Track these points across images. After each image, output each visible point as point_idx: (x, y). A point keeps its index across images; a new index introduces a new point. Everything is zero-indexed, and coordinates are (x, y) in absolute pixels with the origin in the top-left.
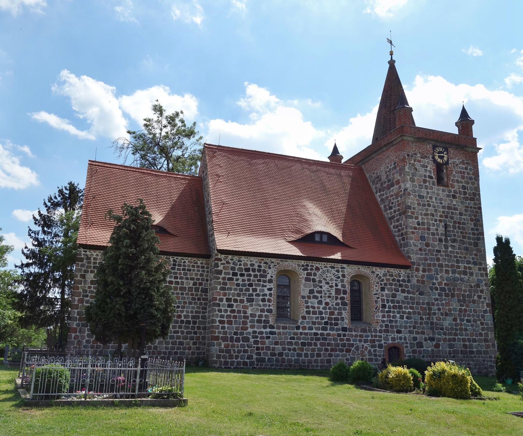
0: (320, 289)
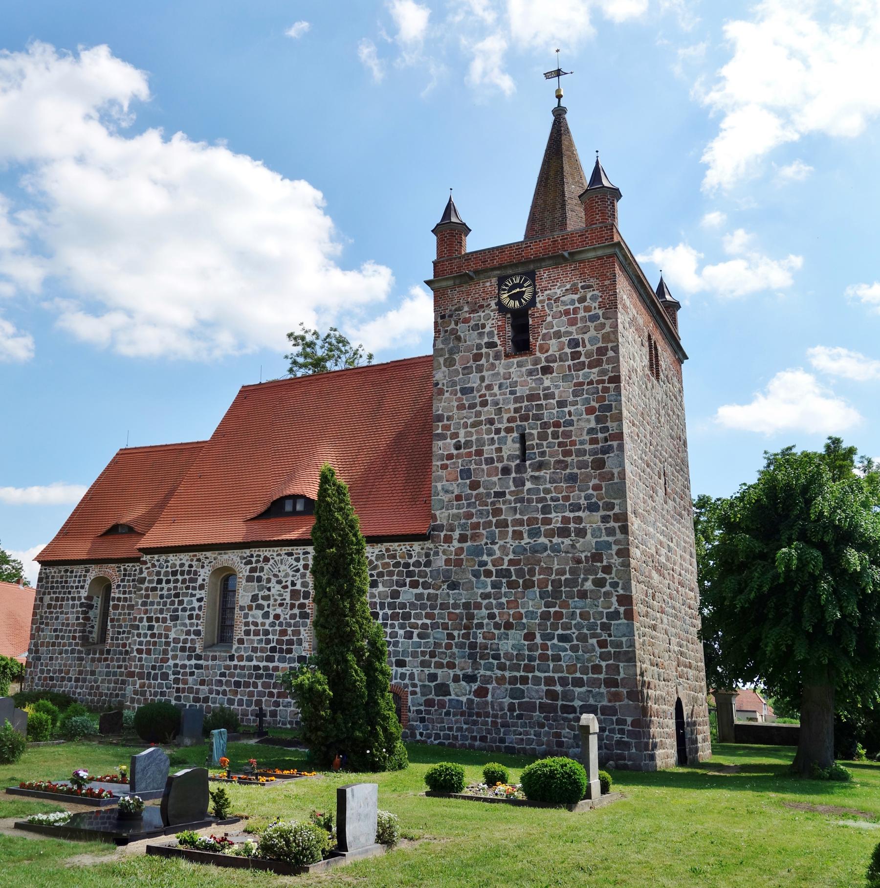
0: (267, 593)
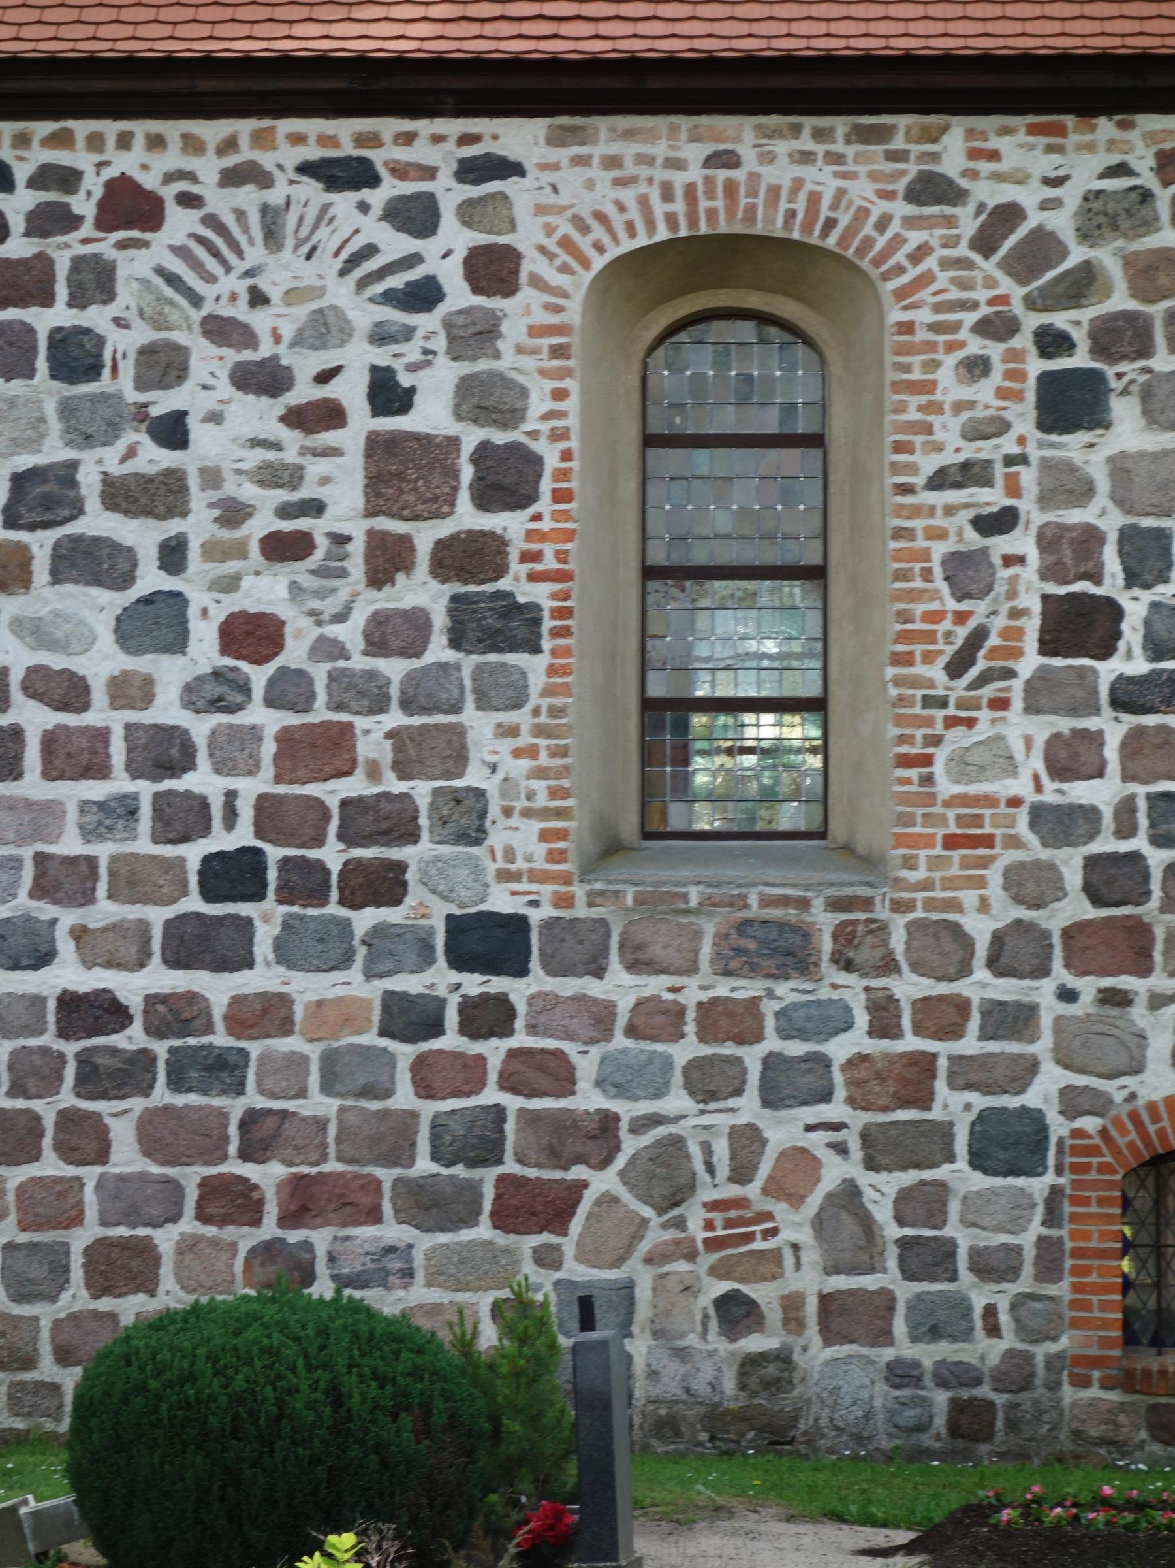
0: (154, 458)
